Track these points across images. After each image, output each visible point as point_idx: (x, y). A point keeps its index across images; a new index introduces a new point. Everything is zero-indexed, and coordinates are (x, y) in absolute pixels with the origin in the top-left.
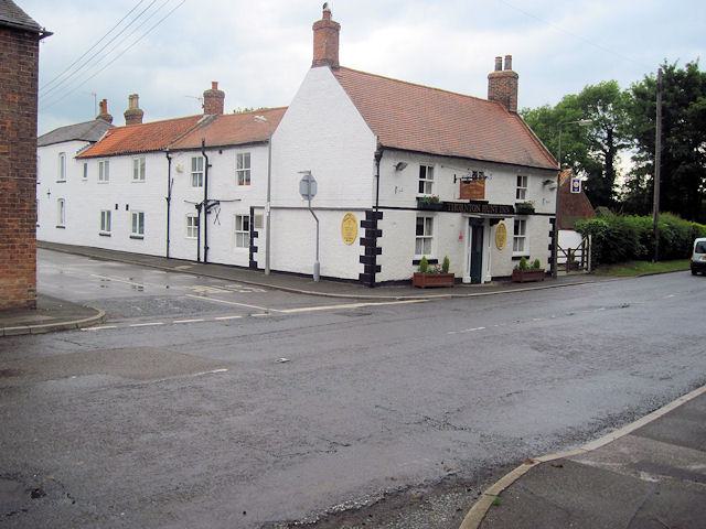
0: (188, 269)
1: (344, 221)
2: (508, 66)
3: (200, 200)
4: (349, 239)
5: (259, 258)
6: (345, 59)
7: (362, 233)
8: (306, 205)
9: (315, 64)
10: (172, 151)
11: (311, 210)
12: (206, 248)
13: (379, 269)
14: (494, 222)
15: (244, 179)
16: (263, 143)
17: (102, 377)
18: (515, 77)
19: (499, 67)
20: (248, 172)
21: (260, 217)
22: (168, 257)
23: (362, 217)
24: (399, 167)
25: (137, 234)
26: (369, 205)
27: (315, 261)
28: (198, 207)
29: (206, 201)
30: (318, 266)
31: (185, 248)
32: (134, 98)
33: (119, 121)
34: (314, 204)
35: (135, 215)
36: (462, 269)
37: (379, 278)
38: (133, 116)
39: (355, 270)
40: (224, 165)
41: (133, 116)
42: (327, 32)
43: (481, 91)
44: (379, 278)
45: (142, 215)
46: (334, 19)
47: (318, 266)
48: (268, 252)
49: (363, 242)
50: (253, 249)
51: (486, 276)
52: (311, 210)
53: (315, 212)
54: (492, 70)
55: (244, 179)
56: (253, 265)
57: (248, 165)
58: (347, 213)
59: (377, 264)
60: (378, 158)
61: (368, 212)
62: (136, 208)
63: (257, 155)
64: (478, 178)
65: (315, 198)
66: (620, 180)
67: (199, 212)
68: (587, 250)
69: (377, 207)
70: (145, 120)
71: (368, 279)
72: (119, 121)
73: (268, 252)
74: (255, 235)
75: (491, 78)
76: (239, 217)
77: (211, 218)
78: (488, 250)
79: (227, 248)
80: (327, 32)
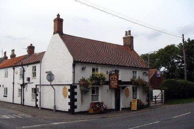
0: (15, 108)
1: (63, 89)
2: (130, 34)
3: (22, 83)
4: (65, 96)
5: (38, 103)
6: (65, 32)
7: (69, 94)
8: (49, 83)
9: (54, 33)
10: (15, 66)
11: (52, 85)
12: (24, 100)
13: (76, 107)
14: (124, 88)
15: (34, 74)
16: (39, 62)
17: (54, 123)
18: (132, 38)
19: (126, 35)
20: (35, 73)
21: (38, 89)
22: (22, 105)
23: (69, 87)
24: (83, 69)
25: (6, 95)
26: (71, 83)
27: (54, 104)
28: (21, 85)
29: (23, 83)
30: (55, 106)
31: (18, 100)
32: (13, 50)
33: (9, 58)
34: (52, 83)
35: (5, 88)
36: (111, 105)
37: (76, 110)
38: (13, 56)
39: (67, 108)
40: (29, 70)
41: (13, 56)
42: (59, 22)
43: (121, 43)
44: (76, 110)
45: (7, 88)
46: (61, 17)
47: (55, 106)
48: (40, 102)
49: (69, 97)
50: (37, 100)
51: (122, 106)
52: (52, 85)
53: (53, 86)
54: (124, 36)
55: (34, 74)
56: (37, 105)
57: (35, 70)
58: (64, 86)
59: (75, 105)
60: (74, 66)
61: (71, 85)
62: (5, 86)
63: (38, 66)
64: (117, 72)
65: (54, 81)
66: (137, 77)
67: (22, 88)
68: (163, 96)
69: (74, 84)
70: (16, 57)
71: (72, 111)
72: (9, 58)
73: (40, 102)
74: (37, 95)
75: (124, 38)
76: (33, 89)
77: (25, 89)
78: (122, 98)
79: (29, 101)
80: (59, 22)
